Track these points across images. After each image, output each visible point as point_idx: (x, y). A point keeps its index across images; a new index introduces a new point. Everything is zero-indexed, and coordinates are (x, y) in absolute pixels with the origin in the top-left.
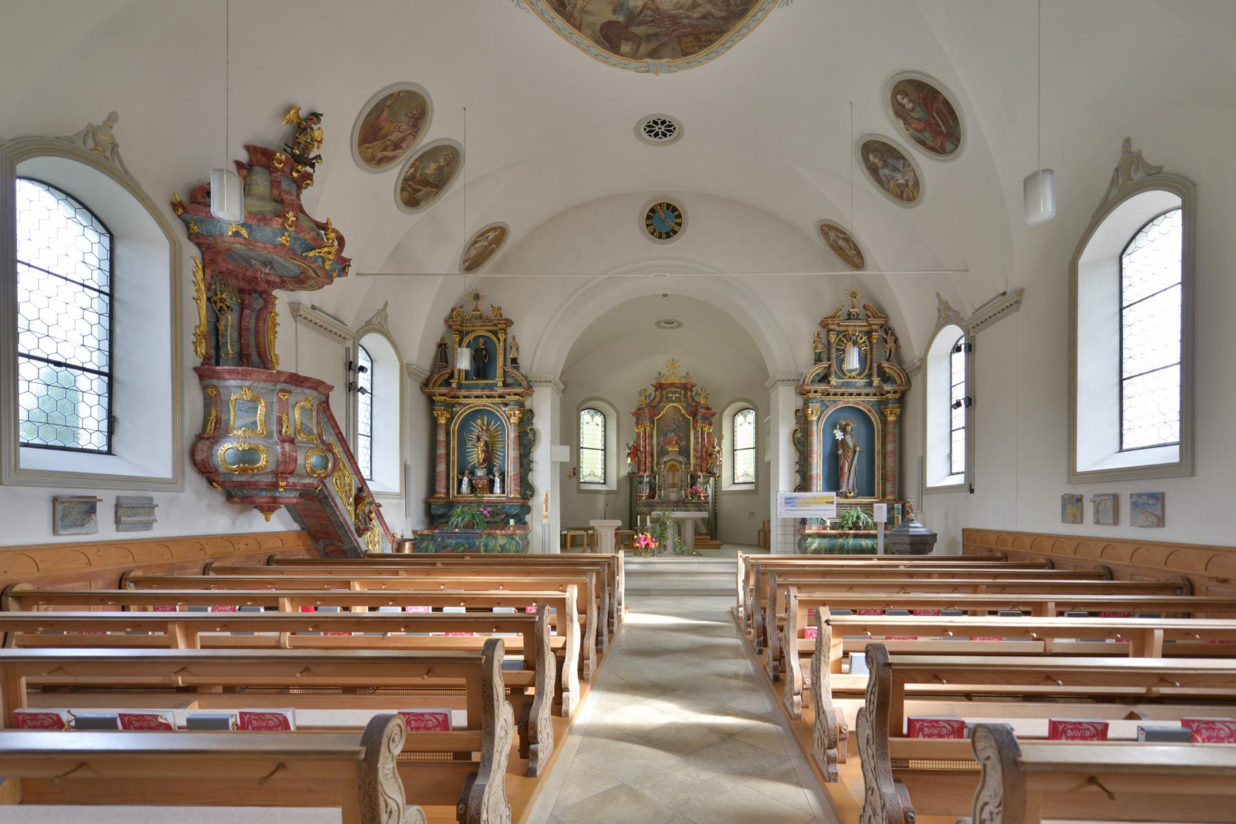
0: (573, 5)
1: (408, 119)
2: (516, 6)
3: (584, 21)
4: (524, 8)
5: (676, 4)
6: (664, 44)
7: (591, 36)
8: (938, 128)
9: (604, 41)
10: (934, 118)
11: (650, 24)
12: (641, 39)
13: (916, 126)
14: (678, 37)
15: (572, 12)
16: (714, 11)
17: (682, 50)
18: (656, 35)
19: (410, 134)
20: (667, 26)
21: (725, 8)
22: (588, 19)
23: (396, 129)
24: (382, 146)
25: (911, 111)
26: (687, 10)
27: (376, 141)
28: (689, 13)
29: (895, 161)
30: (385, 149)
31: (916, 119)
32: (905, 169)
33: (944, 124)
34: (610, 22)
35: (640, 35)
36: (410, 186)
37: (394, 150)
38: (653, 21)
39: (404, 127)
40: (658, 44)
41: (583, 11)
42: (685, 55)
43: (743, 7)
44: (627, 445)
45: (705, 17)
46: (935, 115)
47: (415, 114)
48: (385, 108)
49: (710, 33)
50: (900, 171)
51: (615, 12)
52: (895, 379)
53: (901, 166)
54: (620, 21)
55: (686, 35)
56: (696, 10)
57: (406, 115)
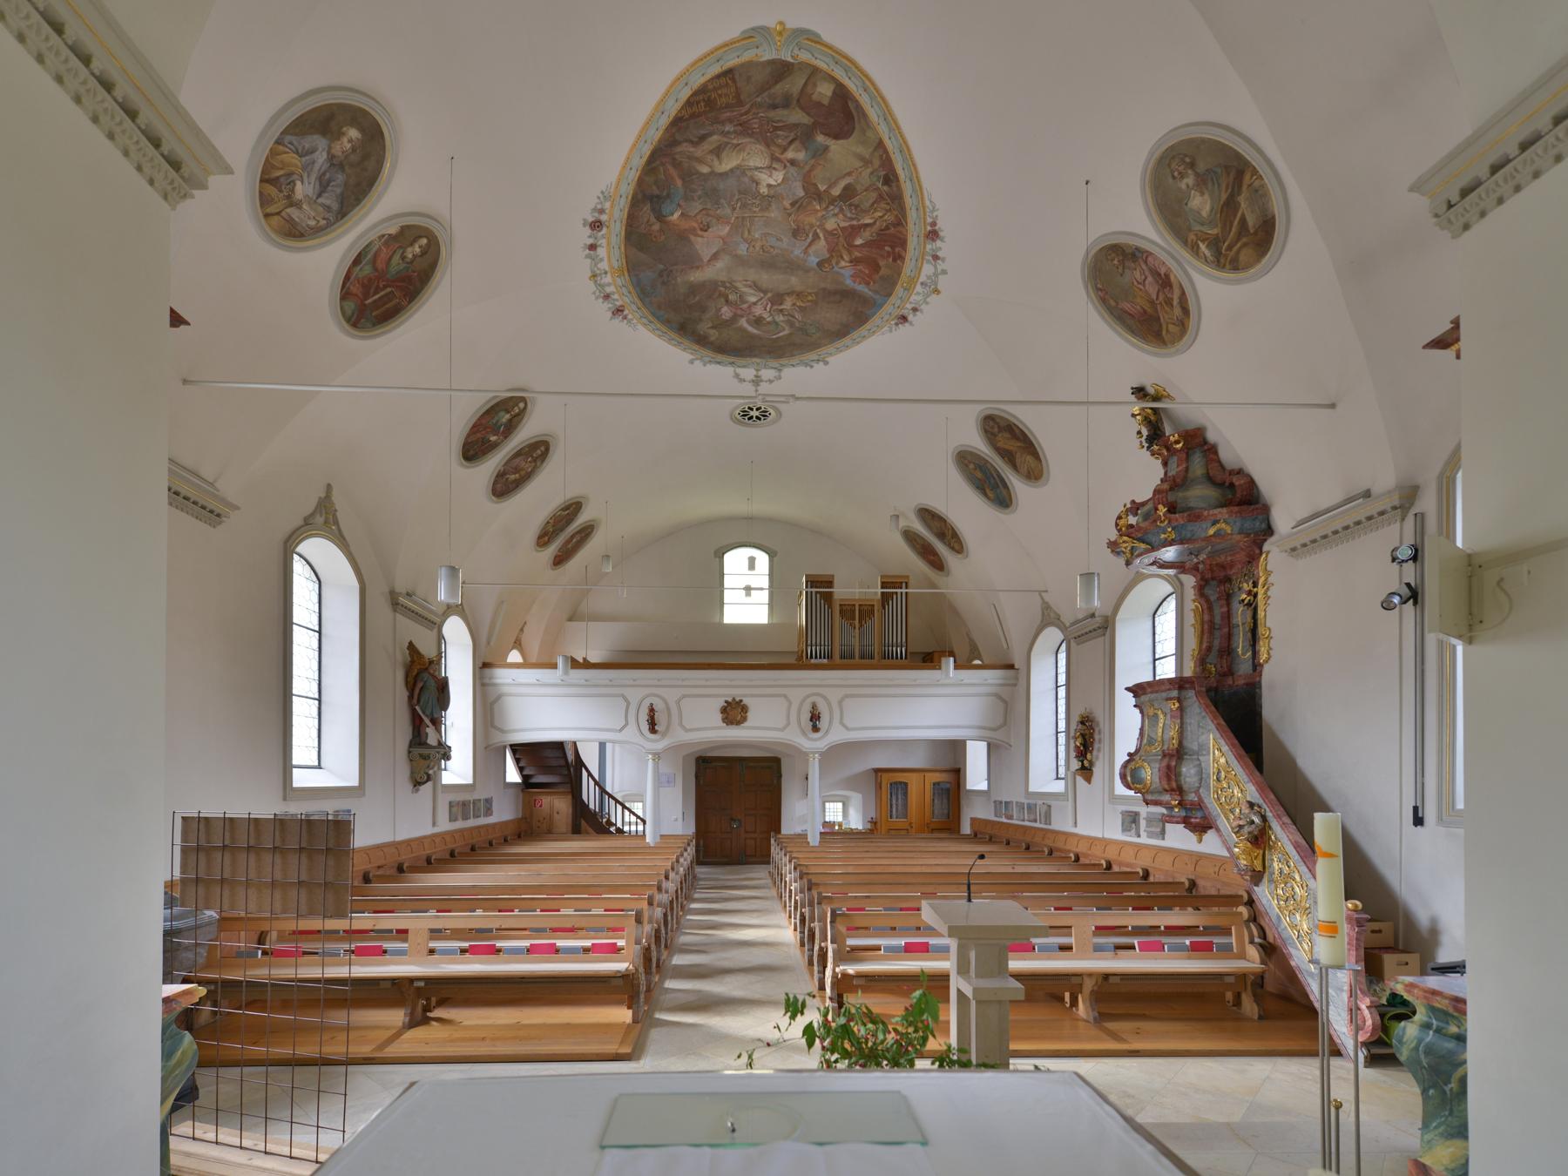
1: (1126, 271)
2: (938, 210)
3: (870, 150)
6: (762, 89)
8: (372, 291)
9: (853, 111)
10: (385, 287)
12: (798, 101)
13: (382, 255)
14: (740, 103)
15: (880, 167)
16: (692, 149)
17: (734, 80)
18: (774, 107)
19: (1146, 262)
21: (677, 156)
22: (865, 152)
23: (1141, 287)
24: (1166, 308)
25: (403, 253)
26: (729, 143)
27: (1159, 318)
28: (726, 140)
29: (339, 191)
30: (1169, 302)
31: (390, 259)
32: (321, 209)
33: (375, 301)
34: (836, 137)
36: (1230, 248)
37: (1171, 286)
38: (776, 128)
39: (1137, 274)
40: (773, 91)
41: (867, 162)
42: (729, 72)
43: (654, 165)
44: (1046, 591)
45: (703, 138)
46: (389, 290)
47: (1119, 261)
48: (1120, 307)
49: (693, 116)
50: (319, 195)
51: (826, 148)
53: (328, 202)
54: (822, 136)
55: (728, 106)
56: (714, 146)
57: (1122, 275)
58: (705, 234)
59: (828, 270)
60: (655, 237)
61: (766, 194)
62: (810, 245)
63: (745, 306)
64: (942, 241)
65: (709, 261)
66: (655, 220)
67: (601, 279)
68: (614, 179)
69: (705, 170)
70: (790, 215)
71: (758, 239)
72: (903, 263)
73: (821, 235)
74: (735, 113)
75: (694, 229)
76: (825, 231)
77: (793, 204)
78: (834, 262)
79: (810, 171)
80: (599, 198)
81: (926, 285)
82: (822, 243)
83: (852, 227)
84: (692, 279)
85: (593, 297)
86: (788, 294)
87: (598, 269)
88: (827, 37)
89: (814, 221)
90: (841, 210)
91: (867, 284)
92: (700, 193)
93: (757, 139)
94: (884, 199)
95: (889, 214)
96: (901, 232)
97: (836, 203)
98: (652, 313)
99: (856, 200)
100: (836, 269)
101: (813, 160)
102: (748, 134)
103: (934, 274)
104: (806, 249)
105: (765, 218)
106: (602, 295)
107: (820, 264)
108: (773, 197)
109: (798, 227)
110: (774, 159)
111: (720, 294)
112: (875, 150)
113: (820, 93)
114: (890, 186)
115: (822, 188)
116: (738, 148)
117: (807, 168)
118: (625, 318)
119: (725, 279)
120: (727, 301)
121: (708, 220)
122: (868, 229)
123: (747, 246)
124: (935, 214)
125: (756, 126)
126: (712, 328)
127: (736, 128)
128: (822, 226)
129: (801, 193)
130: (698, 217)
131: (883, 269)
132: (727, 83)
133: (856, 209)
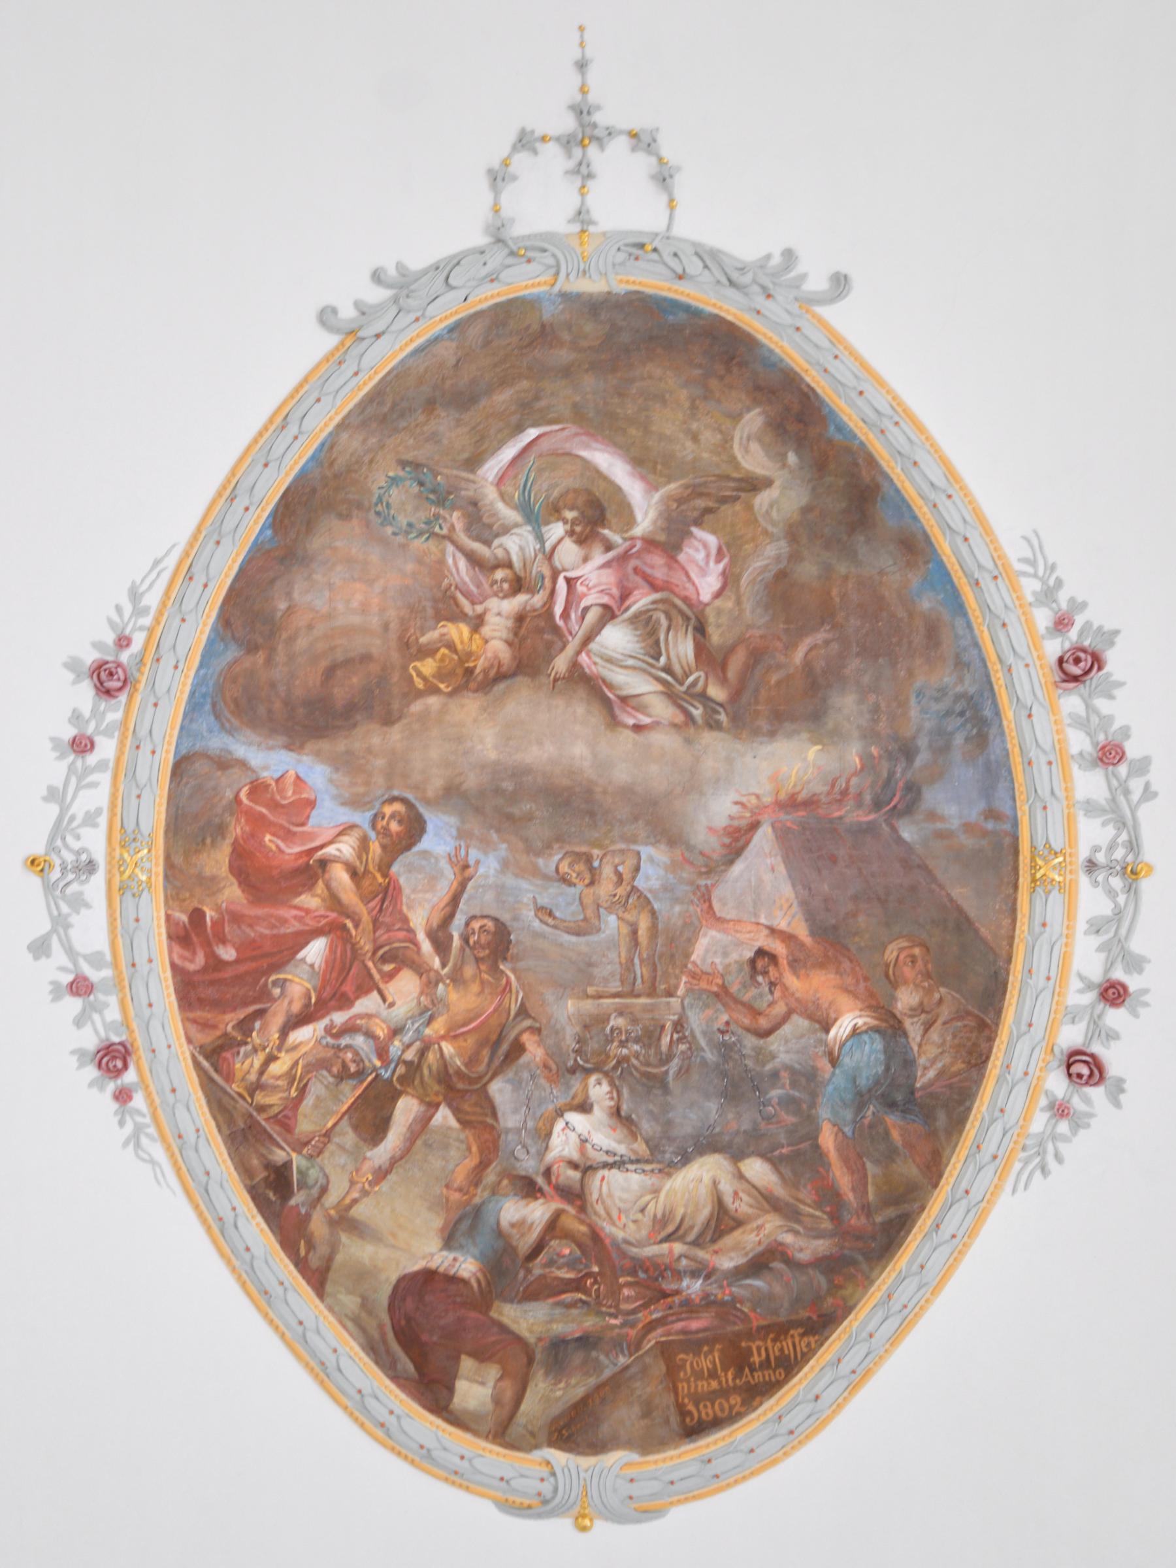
0: (315, 1192)
2: (126, 1144)
3: (339, 1258)
4: (153, 1162)
5: (661, 1222)
6: (616, 1384)
7: (356, 1321)
11: (567, 1297)
12: (530, 1361)
15: (308, 1216)
16: (788, 1238)
17: (683, 1413)
18: (586, 1342)
20: (625, 1307)
21: (827, 1225)
28: (701, 1254)
34: (429, 1276)
35: (531, 1339)
38: (577, 1285)
40: (592, 1381)
41: (344, 1221)
42: (693, 1430)
43: (891, 1212)
45: (758, 1265)
49: (780, 1330)
51: (449, 1241)
52: (448, 961)
54: (465, 1274)
55: (694, 1344)
58: (762, 940)
59: (388, 810)
60: (914, 960)
61: (593, 1079)
62: (455, 900)
63: (642, 600)
64: (80, 1053)
65: (754, 826)
66: (907, 1023)
67: (1112, 847)
68: (1005, 1199)
69: (757, 1169)
70: (523, 1012)
71: (609, 910)
72: (168, 918)
73: (426, 946)
74: (679, 1325)
75: (794, 964)
76: (420, 969)
77: (518, 1049)
78: (375, 848)
79: (483, 1166)
80: (1059, 1158)
81: (77, 869)
82: (420, 919)
83: (344, 1002)
84: (813, 751)
85: (1155, 776)
86: (501, 677)
87: (1111, 893)
88: (486, 1509)
89: (453, 996)
90: (382, 1053)
91: (258, 788)
92: (775, 1093)
93: (624, 1255)
94: (275, 1119)
95: (253, 1077)
96: (205, 1026)
97: (401, 1070)
98: (964, 614)
99: (350, 1093)
100: (362, 819)
101: (477, 1200)
102: (646, 1271)
103: (67, 926)
104: (463, 886)
105: (591, 990)
106: (1123, 769)
107: (414, 828)
108: (572, 1071)
109: (495, 970)
110: (575, 1196)
111: (724, 667)
112: (330, 1259)
113: (483, 1384)
114: (268, 1166)
115: (444, 1116)
116: (670, 1228)
117: (490, 1177)
118: (1062, 623)
119: (709, 738)
120: (700, 630)
121: (753, 991)
122: (296, 1007)
123: (640, 883)
124: (129, 1127)
125: (626, 1292)
126: (754, 485)
127: (674, 1286)
128: (430, 983)
129: (499, 1090)
130: (780, 1009)
131: (224, 870)
132: (697, 1406)
133: (344, 1066)
